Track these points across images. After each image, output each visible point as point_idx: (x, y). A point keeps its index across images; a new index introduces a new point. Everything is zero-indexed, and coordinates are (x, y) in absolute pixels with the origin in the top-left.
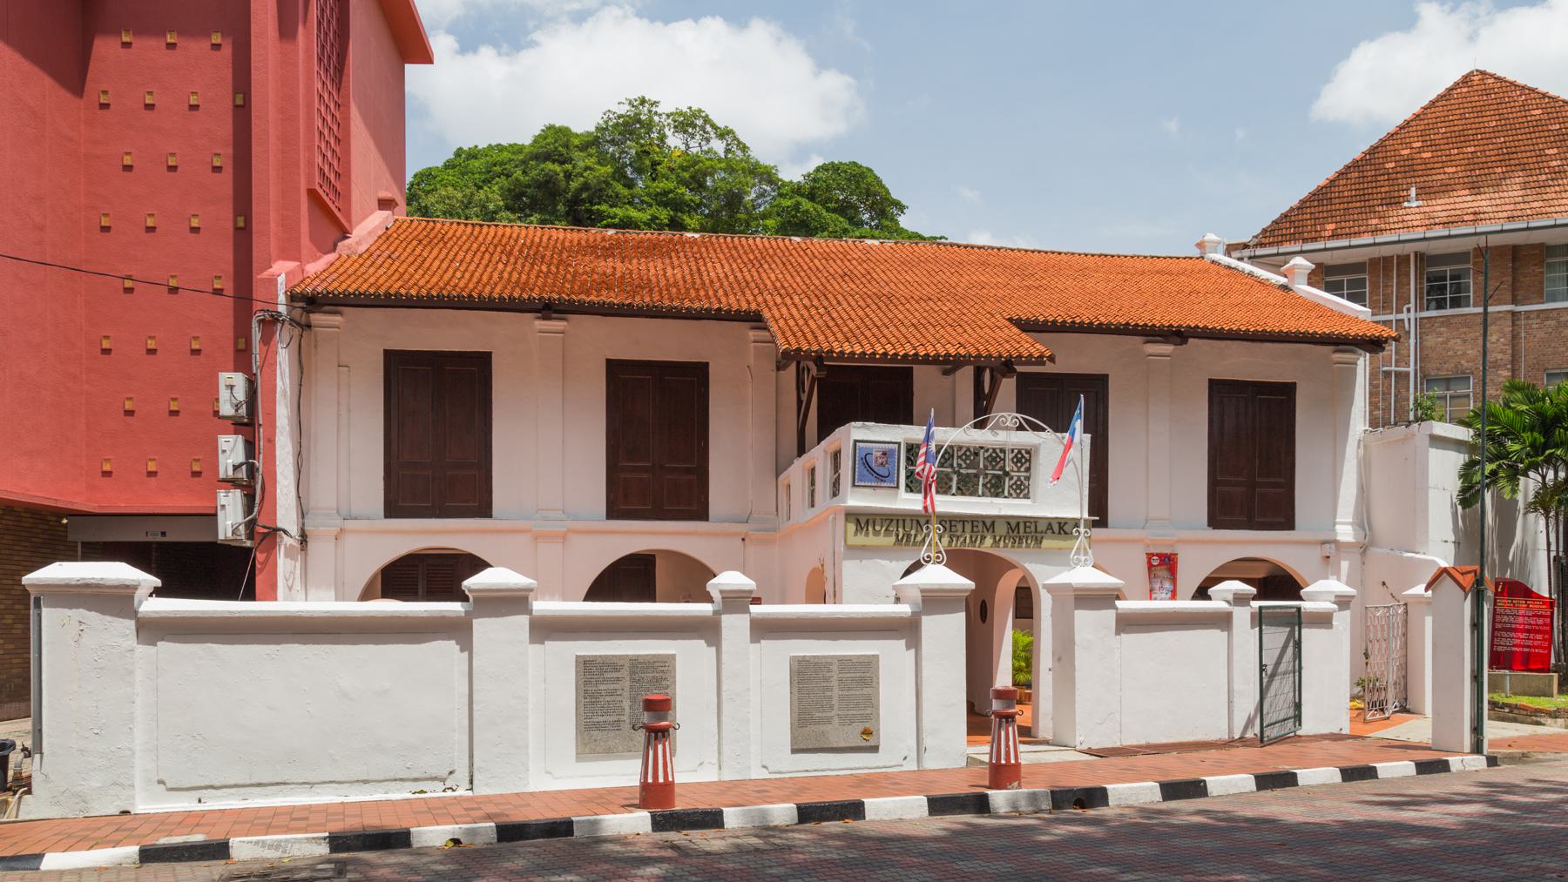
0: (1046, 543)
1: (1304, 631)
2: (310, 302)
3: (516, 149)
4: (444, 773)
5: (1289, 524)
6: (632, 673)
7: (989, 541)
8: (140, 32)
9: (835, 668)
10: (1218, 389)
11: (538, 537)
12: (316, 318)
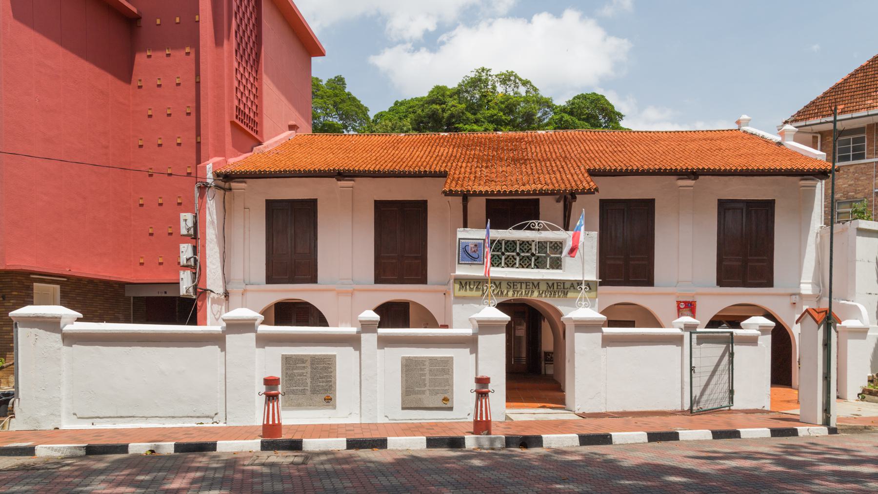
0: (570, 295)
1: (735, 347)
2: (227, 178)
3: (421, 99)
4: (212, 414)
5: (770, 283)
6: (312, 364)
7: (536, 294)
8: (154, 49)
9: (427, 363)
10: (724, 206)
11: (339, 293)
12: (234, 185)
